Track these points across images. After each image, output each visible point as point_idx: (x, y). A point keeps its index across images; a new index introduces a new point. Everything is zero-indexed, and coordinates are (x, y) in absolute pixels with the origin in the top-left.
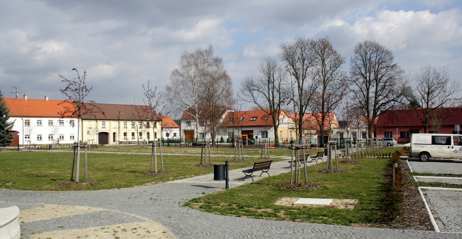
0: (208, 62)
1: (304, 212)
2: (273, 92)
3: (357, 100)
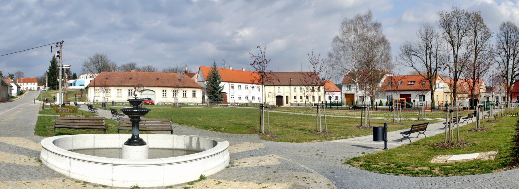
0: (367, 27)
1: (456, 167)
2: (430, 58)
3: (500, 70)
